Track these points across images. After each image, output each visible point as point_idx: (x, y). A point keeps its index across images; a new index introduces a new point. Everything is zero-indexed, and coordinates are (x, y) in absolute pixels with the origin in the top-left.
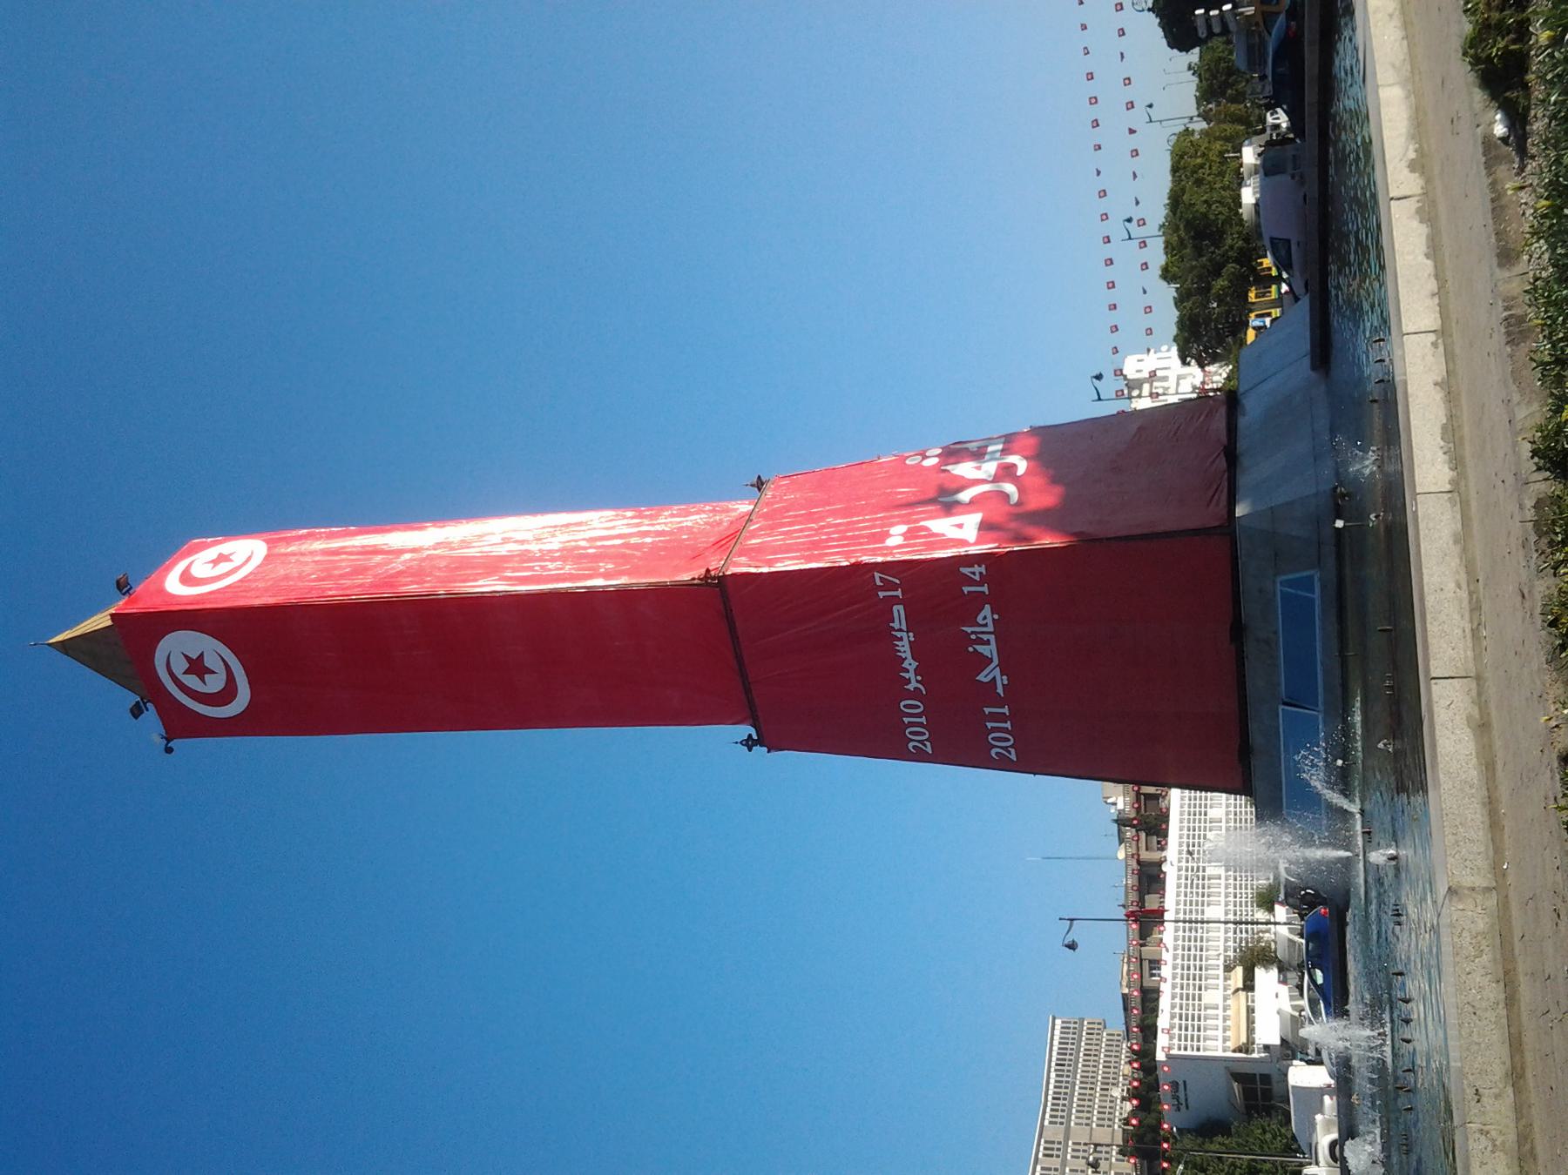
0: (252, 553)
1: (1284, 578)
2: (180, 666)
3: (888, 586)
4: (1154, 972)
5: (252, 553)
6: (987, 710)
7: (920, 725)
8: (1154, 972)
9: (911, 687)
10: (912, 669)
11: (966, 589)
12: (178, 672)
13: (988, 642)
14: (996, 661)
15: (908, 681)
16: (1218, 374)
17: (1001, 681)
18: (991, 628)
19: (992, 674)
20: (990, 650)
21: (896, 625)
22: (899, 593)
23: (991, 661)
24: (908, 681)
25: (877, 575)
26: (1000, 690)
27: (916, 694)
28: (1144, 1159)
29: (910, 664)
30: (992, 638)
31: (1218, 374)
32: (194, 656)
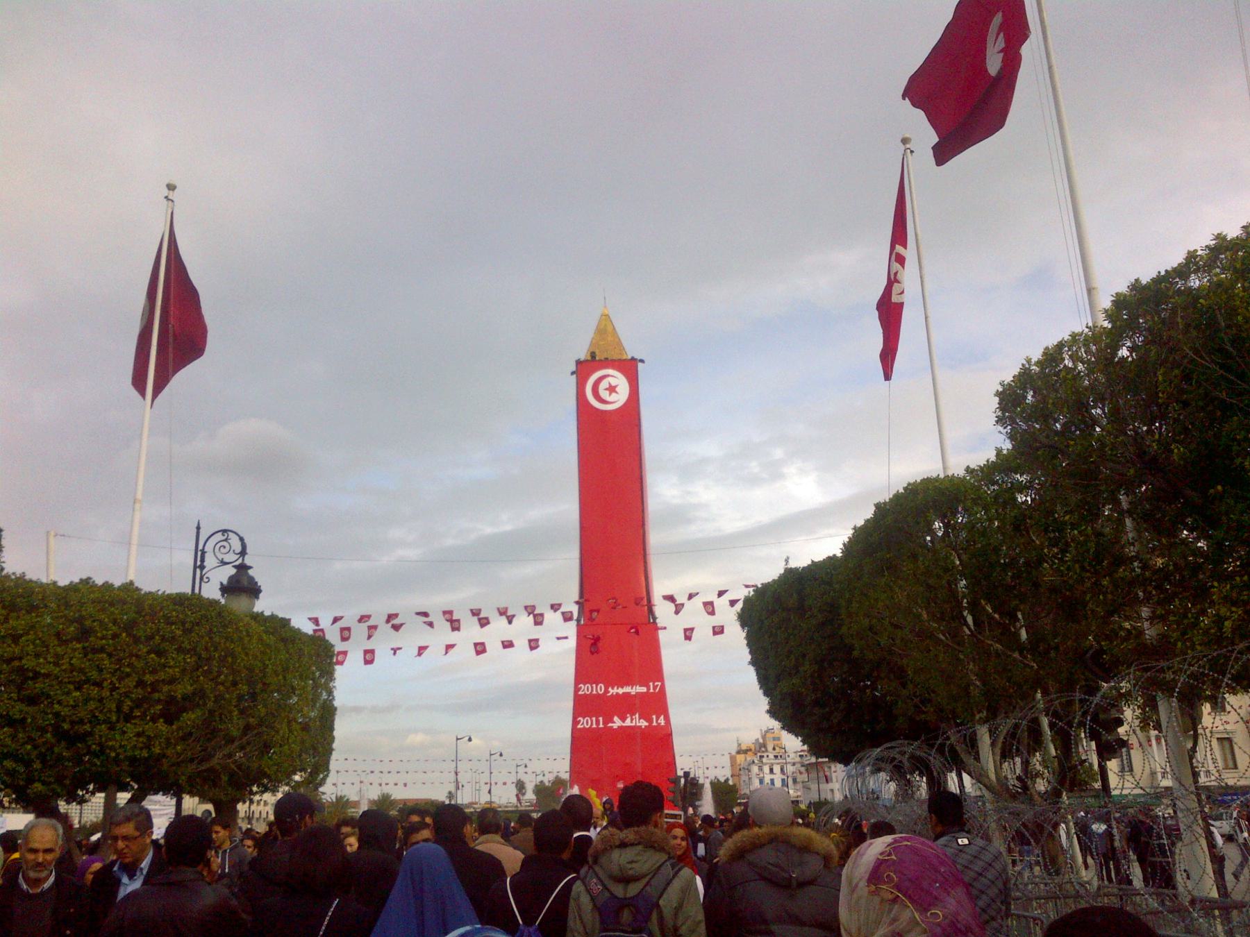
0: (698, 594)
1: (923, 708)
2: (613, 381)
3: (655, 687)
4: (1163, 740)
5: (698, 594)
6: (601, 719)
7: (592, 690)
8: (1163, 740)
9: (610, 689)
10: (618, 691)
11: (654, 717)
12: (610, 379)
13: (632, 722)
14: (624, 725)
15: (613, 689)
16: (131, 769)
17: (615, 726)
18: (638, 724)
19: (617, 723)
20: (628, 723)
21: (638, 687)
22: (652, 691)
23: (624, 722)
24: (613, 689)
25: (660, 684)
26: (610, 725)
27: (606, 691)
28: (1091, 740)
29: (621, 691)
30: (634, 724)
31: (131, 769)
32: (617, 389)
